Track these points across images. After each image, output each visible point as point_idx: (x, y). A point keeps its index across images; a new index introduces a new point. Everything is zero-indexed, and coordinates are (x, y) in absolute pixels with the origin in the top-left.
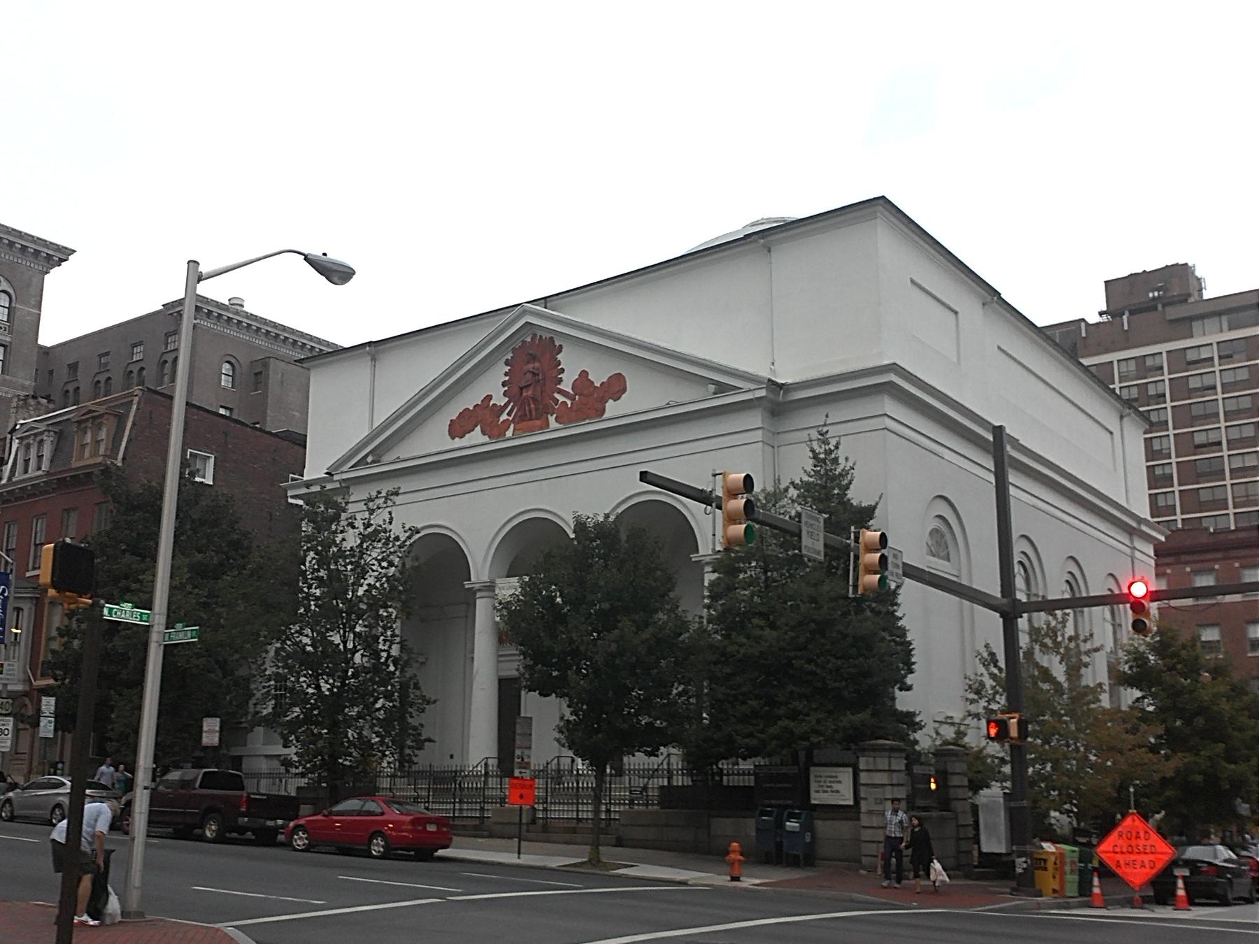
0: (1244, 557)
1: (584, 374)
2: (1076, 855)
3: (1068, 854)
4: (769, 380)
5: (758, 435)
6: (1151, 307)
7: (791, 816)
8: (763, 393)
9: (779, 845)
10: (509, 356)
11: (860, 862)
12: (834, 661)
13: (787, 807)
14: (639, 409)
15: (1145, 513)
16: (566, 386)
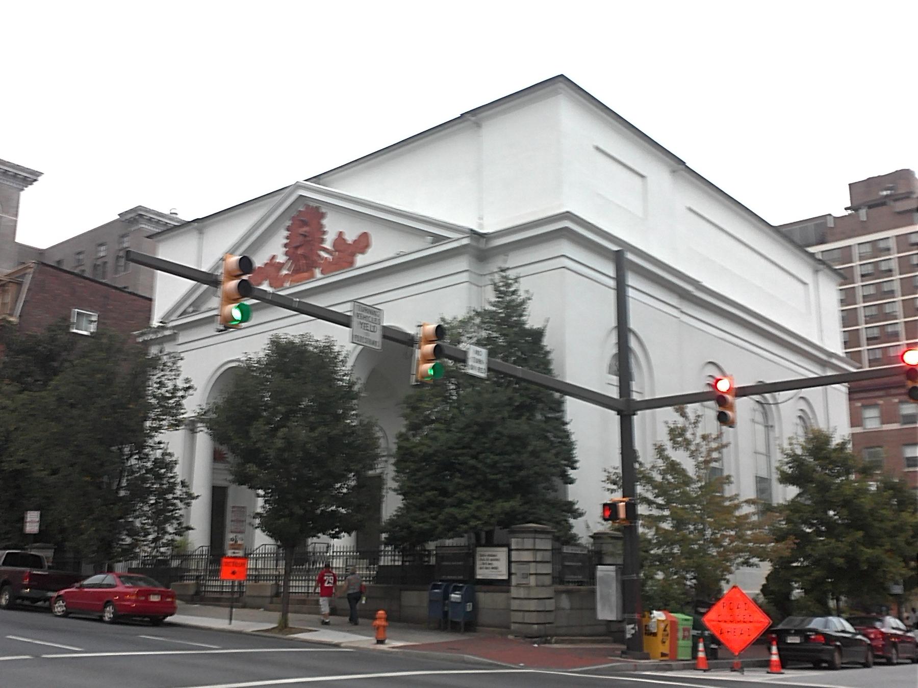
0: (866, 398)
1: (341, 233)
2: (691, 623)
3: (680, 622)
4: (472, 230)
5: (464, 277)
6: (882, 203)
7: (456, 589)
8: (465, 241)
9: (446, 614)
10: (288, 223)
11: (508, 627)
12: (492, 457)
13: (454, 581)
14: (379, 259)
15: (840, 351)
16: (328, 245)
